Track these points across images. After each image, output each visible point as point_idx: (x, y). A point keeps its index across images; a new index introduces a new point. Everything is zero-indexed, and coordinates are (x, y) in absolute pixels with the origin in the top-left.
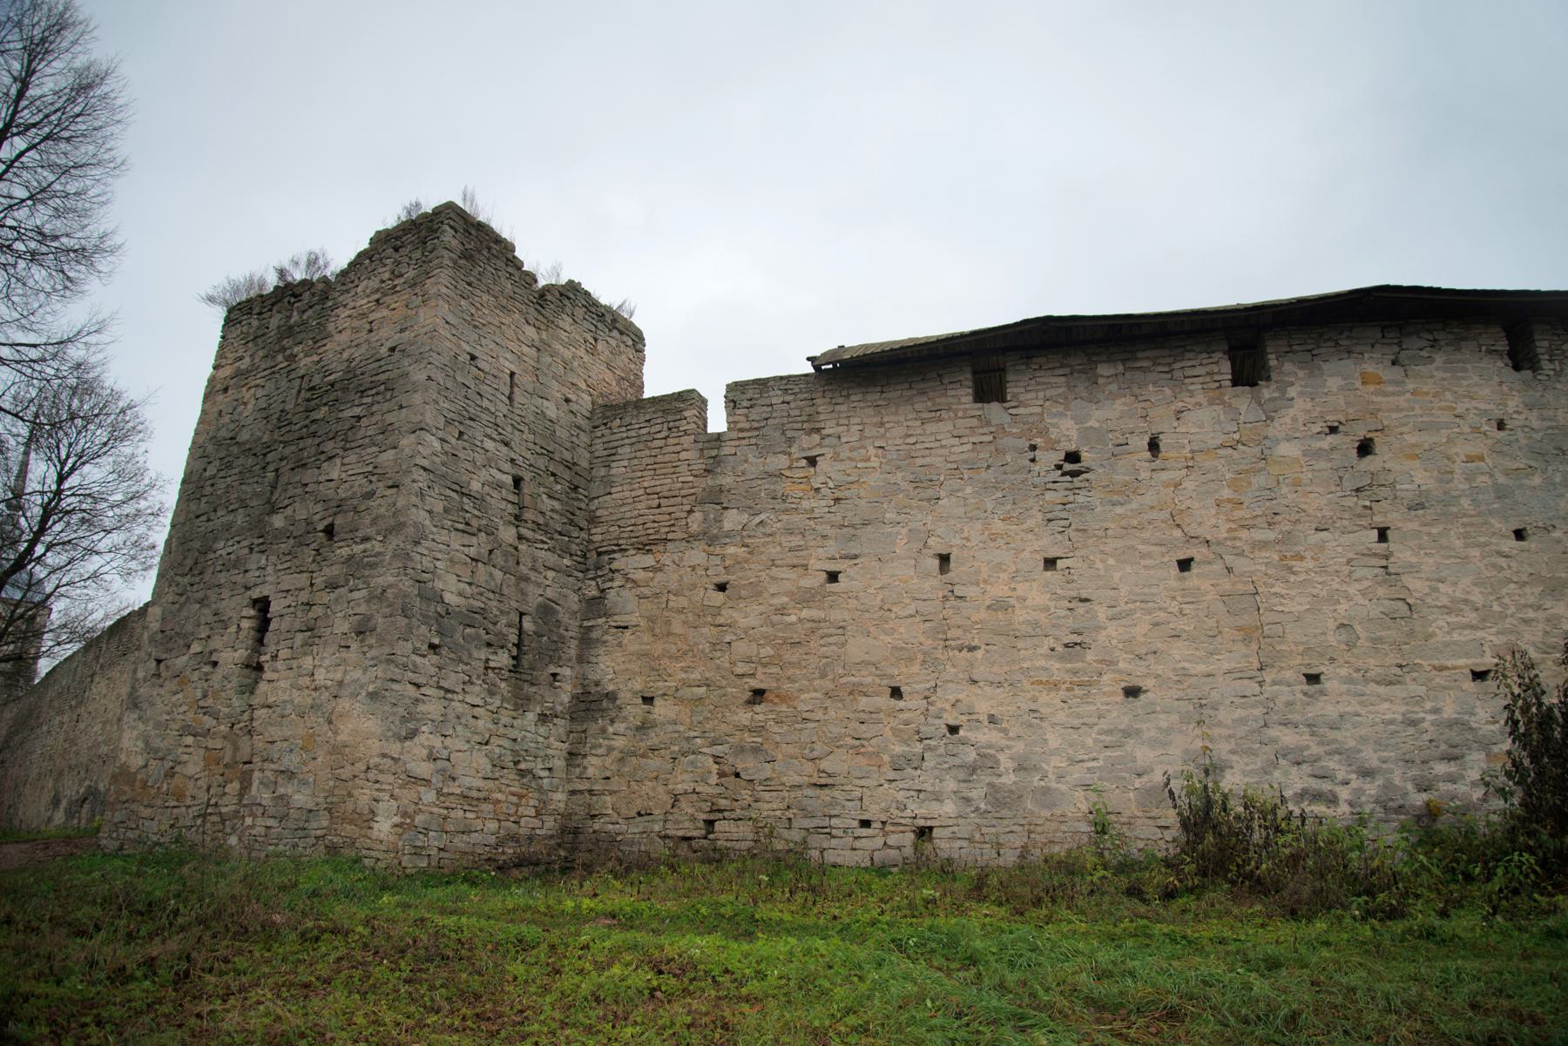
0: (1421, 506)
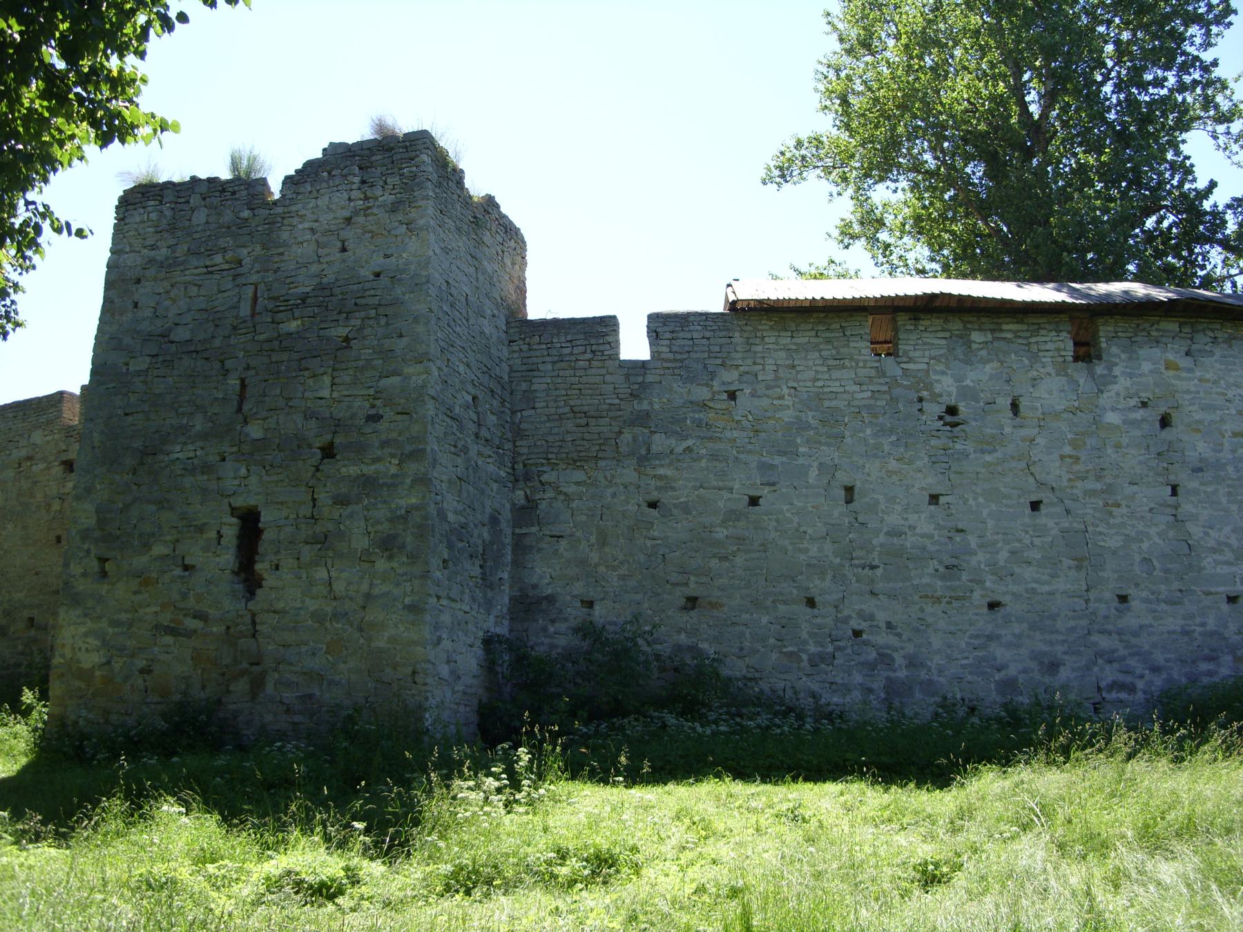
0: (1200, 470)
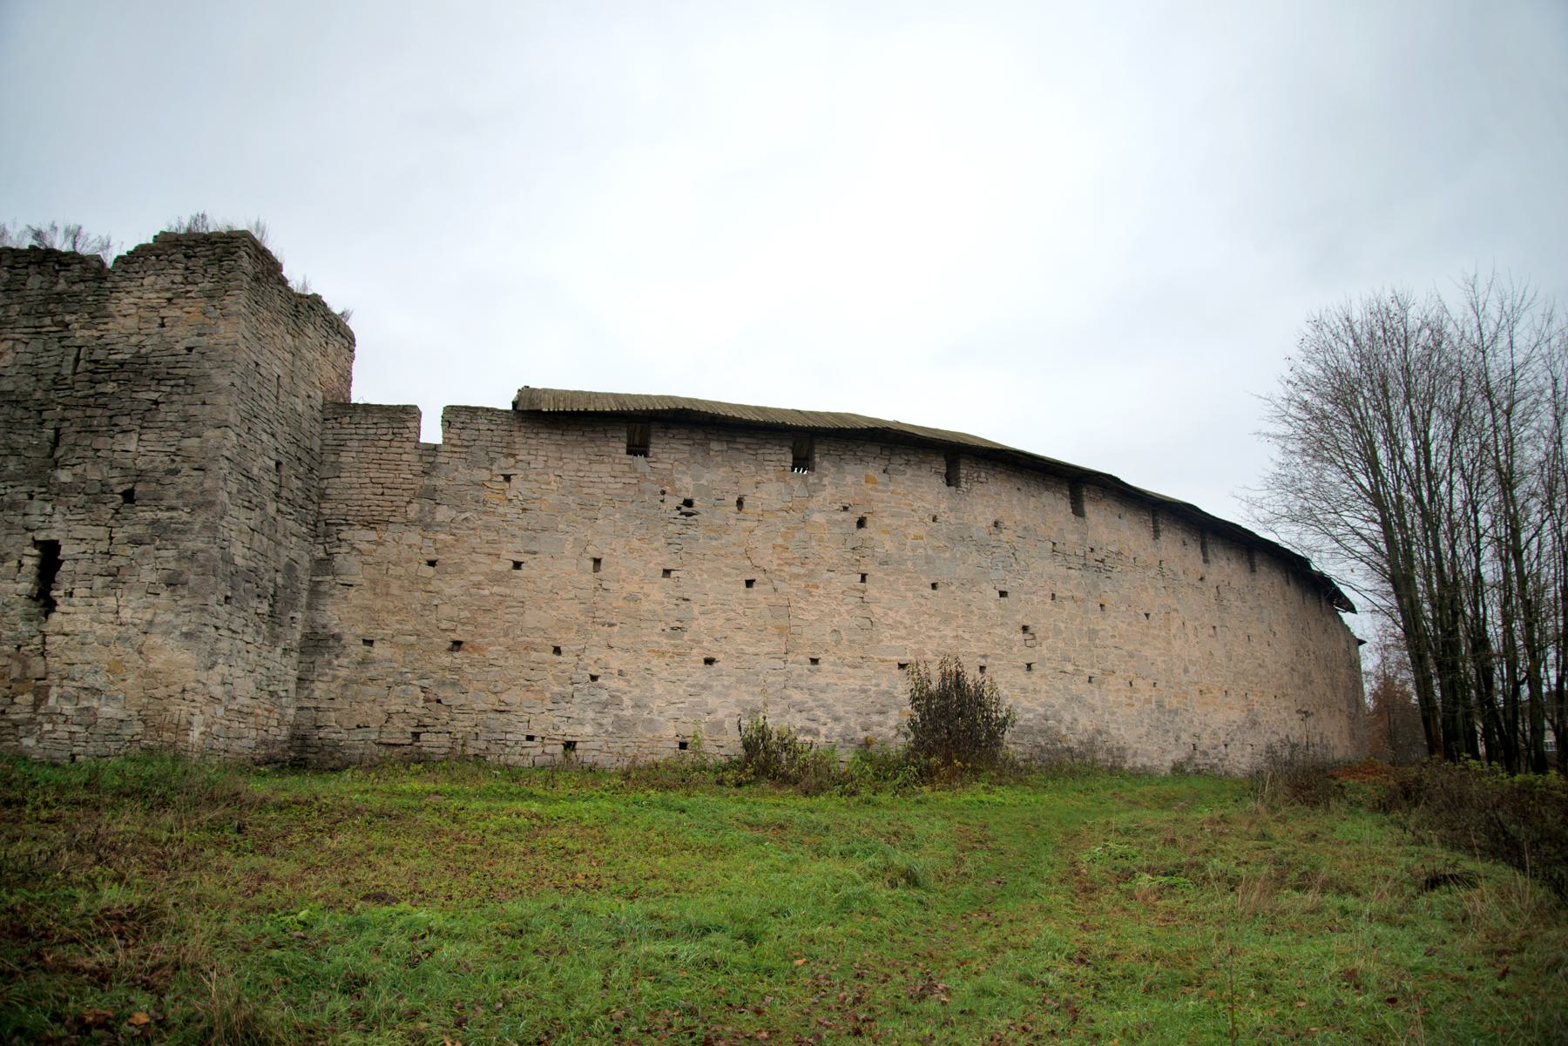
0: (886, 563)
